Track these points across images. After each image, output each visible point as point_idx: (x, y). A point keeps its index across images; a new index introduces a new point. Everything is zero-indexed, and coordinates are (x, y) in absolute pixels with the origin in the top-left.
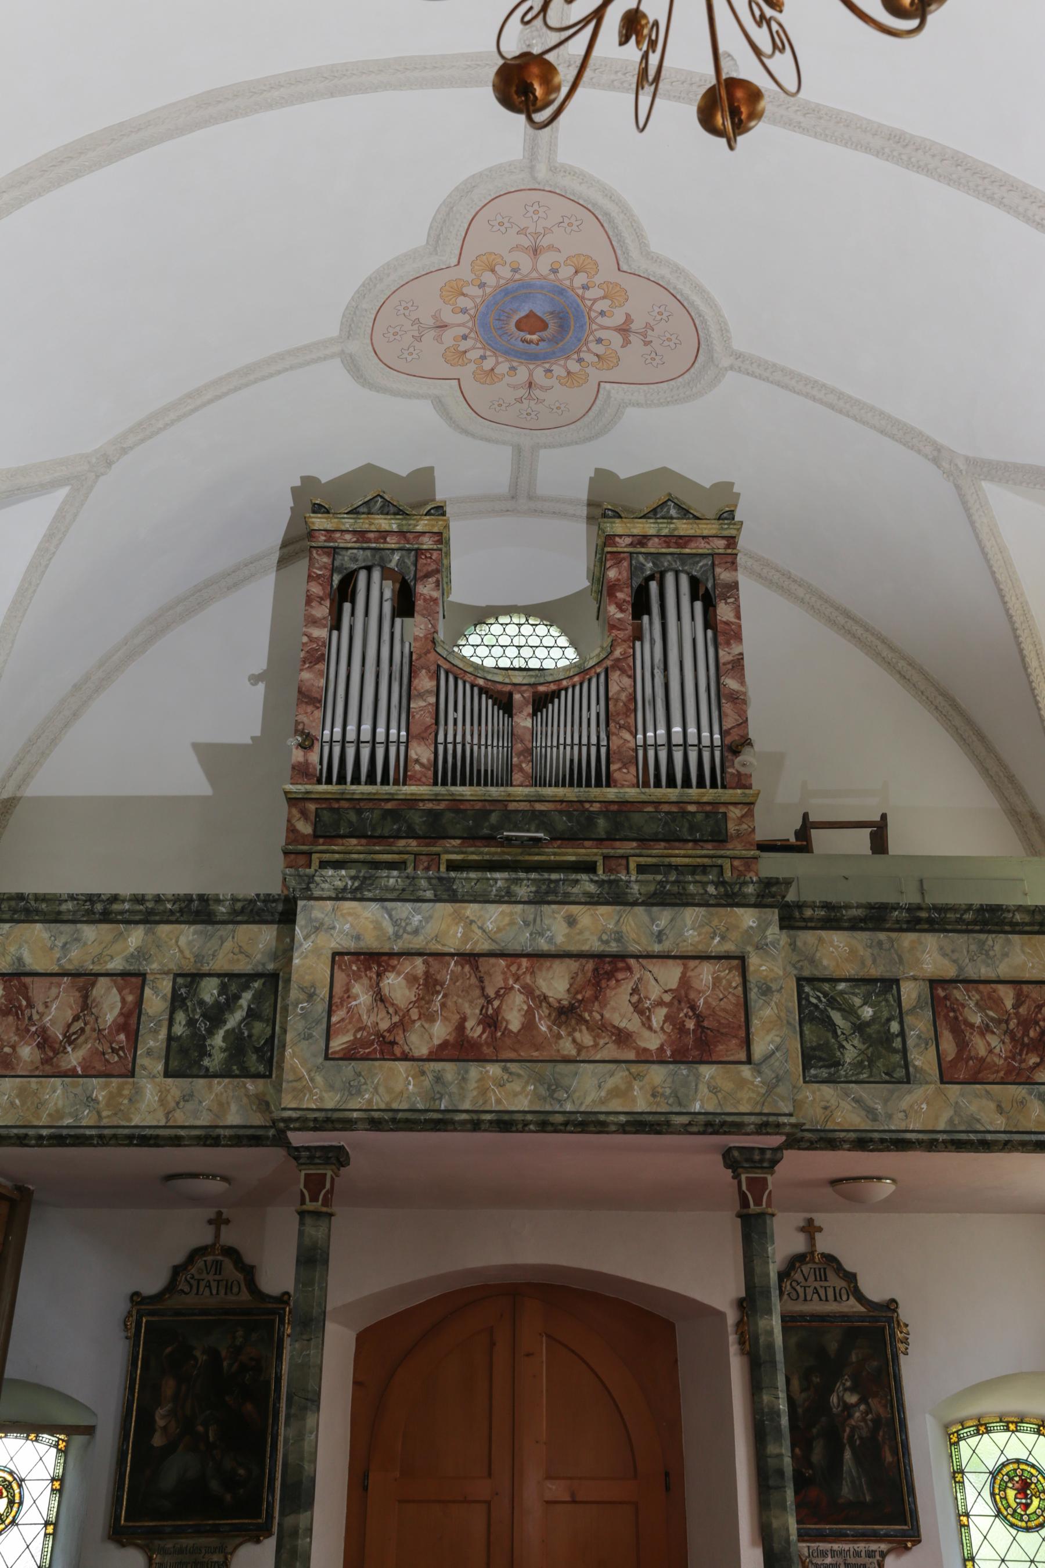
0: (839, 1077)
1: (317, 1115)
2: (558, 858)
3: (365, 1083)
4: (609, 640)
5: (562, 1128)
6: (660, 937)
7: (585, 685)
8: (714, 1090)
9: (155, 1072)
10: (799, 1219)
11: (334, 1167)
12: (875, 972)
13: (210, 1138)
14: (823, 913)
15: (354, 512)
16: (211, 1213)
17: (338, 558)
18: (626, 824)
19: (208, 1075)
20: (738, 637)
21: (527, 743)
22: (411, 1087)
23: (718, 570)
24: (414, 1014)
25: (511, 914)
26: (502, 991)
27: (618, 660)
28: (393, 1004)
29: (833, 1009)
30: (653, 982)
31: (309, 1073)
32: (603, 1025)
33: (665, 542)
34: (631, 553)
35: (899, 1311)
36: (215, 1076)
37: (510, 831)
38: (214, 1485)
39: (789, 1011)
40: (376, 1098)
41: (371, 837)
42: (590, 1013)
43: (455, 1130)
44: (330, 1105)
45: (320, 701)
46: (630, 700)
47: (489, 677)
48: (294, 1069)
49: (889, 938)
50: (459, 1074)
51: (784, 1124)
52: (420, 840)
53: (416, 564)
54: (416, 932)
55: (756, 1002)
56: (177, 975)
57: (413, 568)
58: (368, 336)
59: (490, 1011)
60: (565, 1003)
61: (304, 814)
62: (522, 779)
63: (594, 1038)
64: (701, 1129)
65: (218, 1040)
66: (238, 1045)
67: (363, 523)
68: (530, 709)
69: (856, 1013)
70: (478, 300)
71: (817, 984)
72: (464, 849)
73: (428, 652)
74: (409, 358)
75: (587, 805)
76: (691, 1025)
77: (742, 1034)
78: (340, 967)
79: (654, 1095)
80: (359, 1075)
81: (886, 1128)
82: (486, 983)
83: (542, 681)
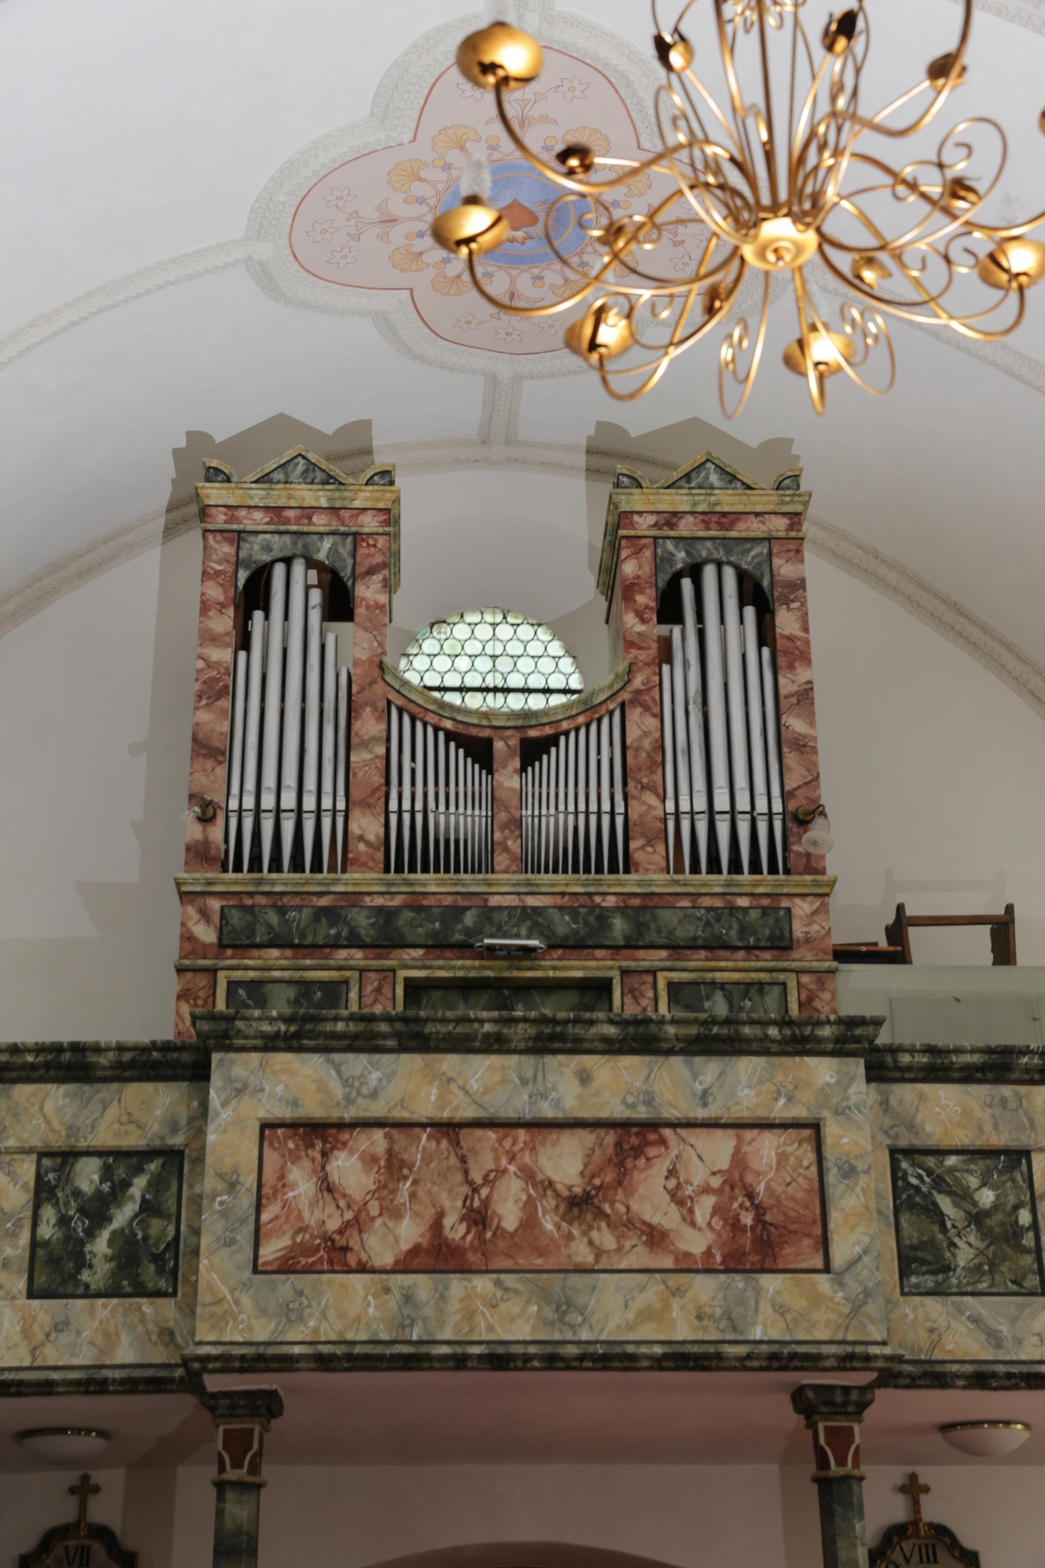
0: (950, 1287)
1: (244, 1350)
2: (559, 974)
3: (309, 1306)
4: (626, 664)
5: (577, 1364)
6: (704, 1098)
7: (593, 728)
8: (781, 1310)
9: (16, 1291)
10: (897, 1474)
11: (264, 1420)
12: (997, 1140)
13: (93, 1384)
14: (925, 1060)
15: (264, 479)
16: (72, 1477)
17: (245, 547)
18: (652, 926)
19: (88, 1294)
20: (805, 658)
21: (513, 811)
22: (371, 1310)
23: (777, 562)
24: (374, 1208)
25: (503, 1068)
26: (492, 1176)
27: (638, 692)
28: (344, 1195)
29: (940, 1192)
30: (696, 1160)
31: (232, 1291)
32: (629, 1220)
33: (703, 521)
34: (655, 538)
36: (98, 1295)
37: (491, 936)
39: (879, 1196)
40: (324, 1326)
41: (300, 946)
42: (612, 1203)
43: (432, 1368)
44: (261, 1336)
45: (223, 754)
46: (655, 749)
47: (460, 718)
48: (211, 1287)
49: (1016, 1094)
50: (436, 1291)
51: (876, 1357)
52: (368, 951)
53: (354, 554)
54: (374, 1095)
55: (835, 1187)
56: (42, 1155)
57: (350, 561)
58: (287, 235)
59: (477, 1203)
60: (578, 1190)
61: (204, 914)
62: (507, 862)
63: (618, 1239)
64: (764, 1364)
65: (101, 1245)
66: (129, 1252)
67: (278, 497)
68: (517, 763)
69: (971, 1198)
70: (441, 187)
71: (919, 1158)
72: (429, 963)
73: (373, 682)
74: (342, 263)
75: (598, 899)
76: (747, 1219)
77: (818, 1231)
78: (271, 1144)
79: (699, 1317)
80: (301, 1294)
81: (1014, 1358)
82: (471, 1164)
83: (533, 723)
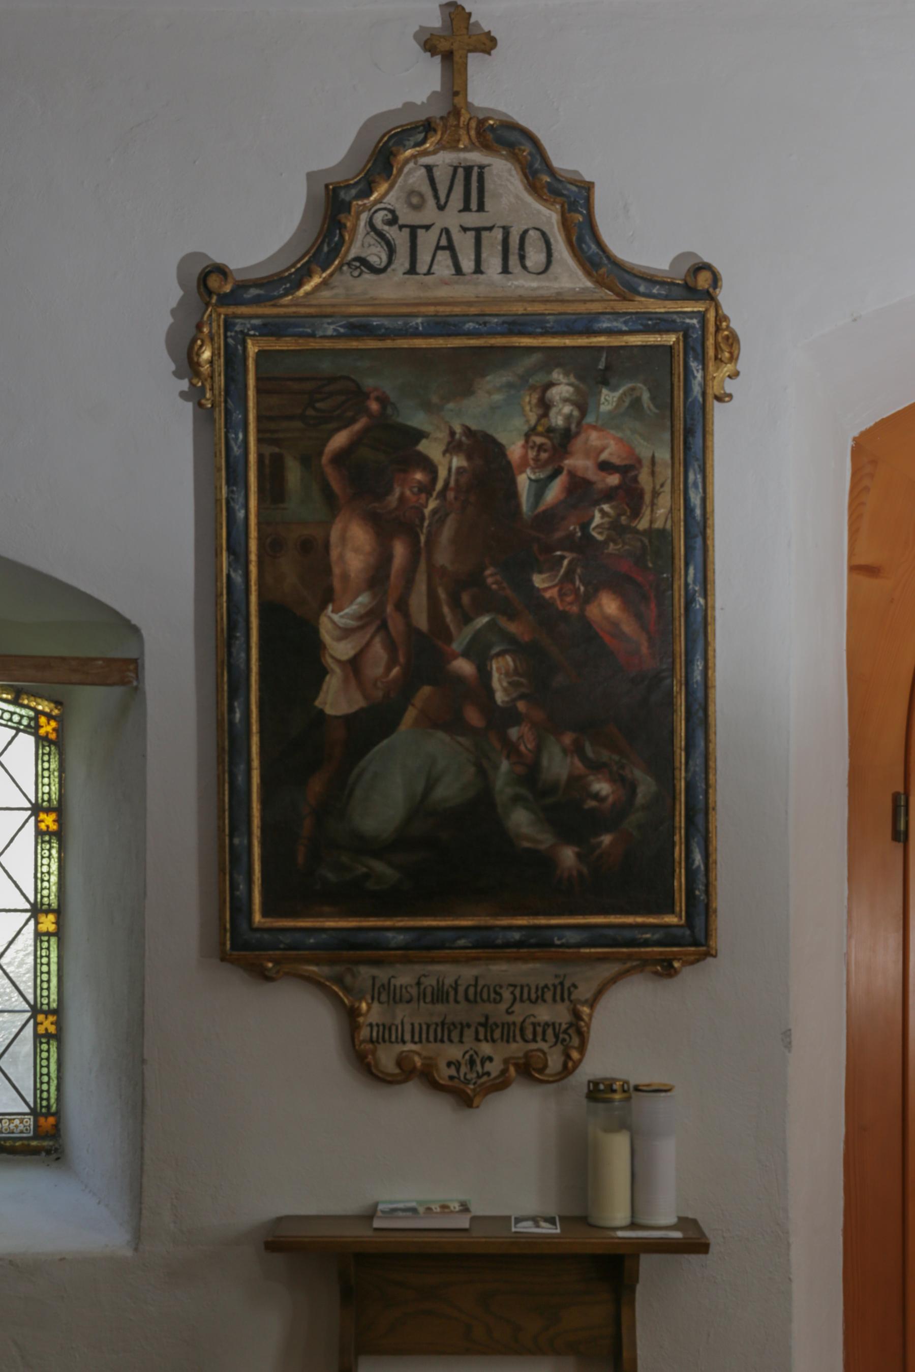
35: (723, 296)
38: (521, 821)
